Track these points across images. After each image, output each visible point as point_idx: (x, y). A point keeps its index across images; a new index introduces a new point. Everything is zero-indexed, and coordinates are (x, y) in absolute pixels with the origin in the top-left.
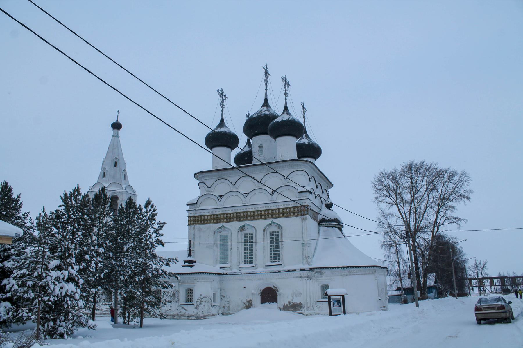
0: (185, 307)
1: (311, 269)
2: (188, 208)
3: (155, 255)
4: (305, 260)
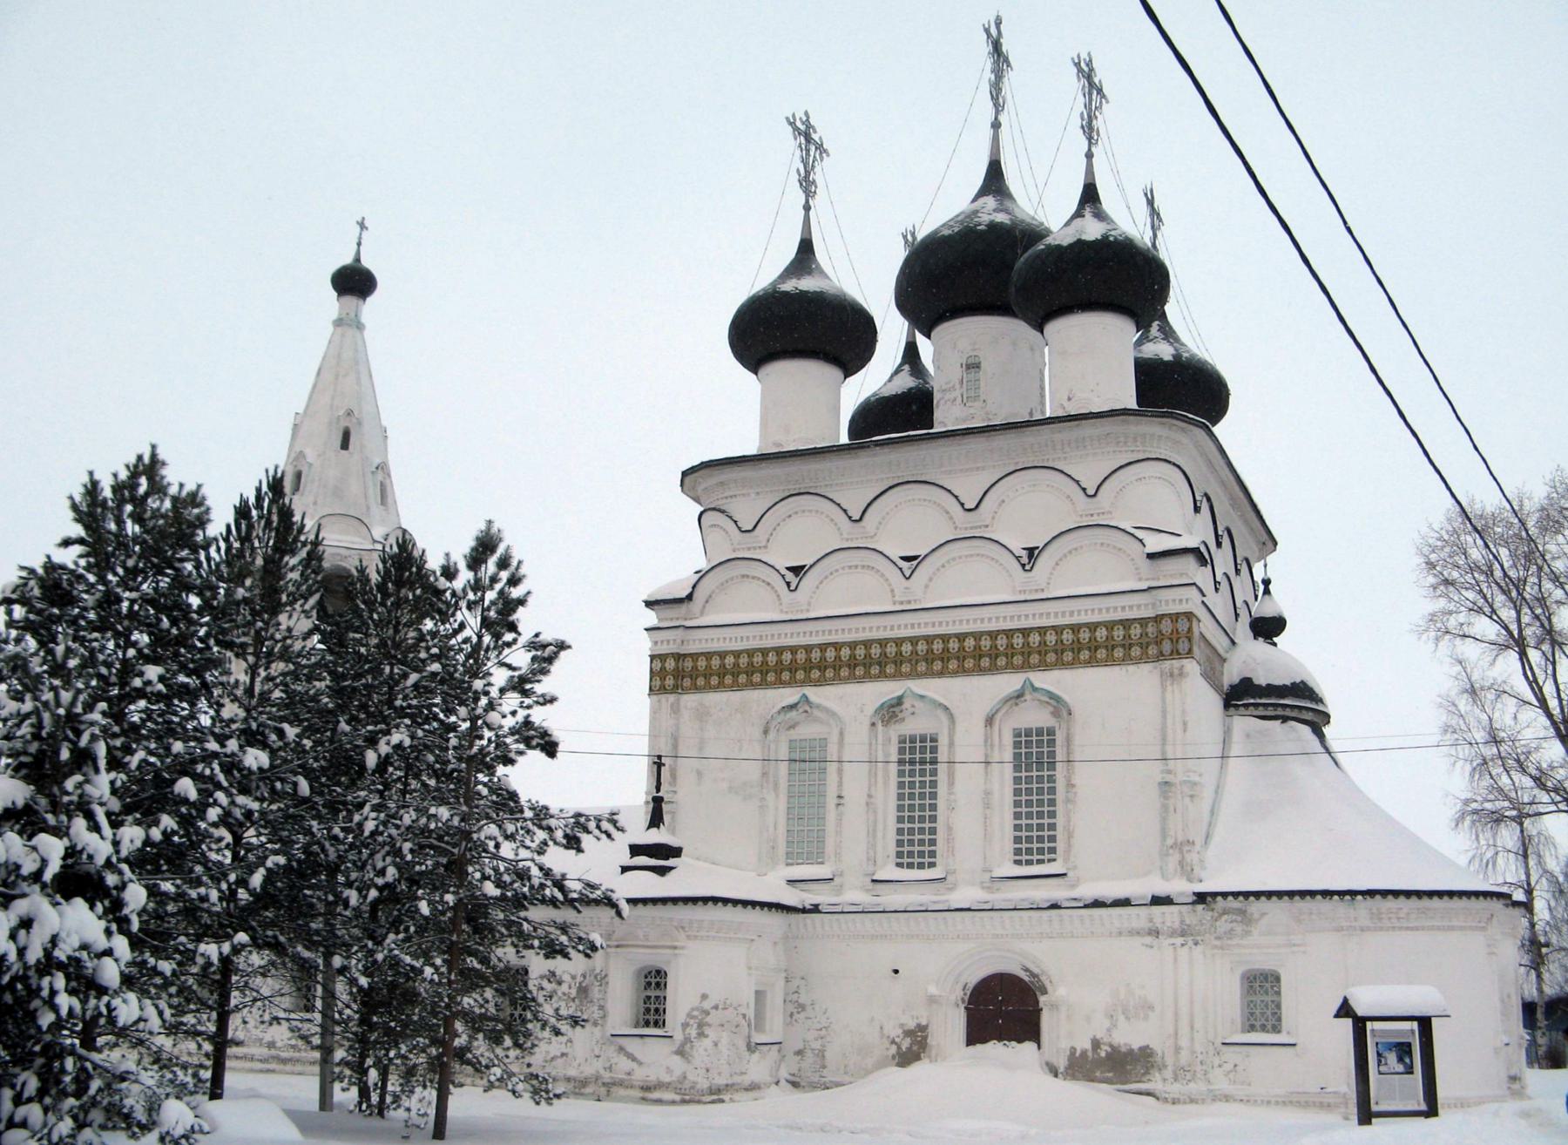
0: (633, 1046)
1: (1201, 898)
2: (651, 618)
3: (513, 796)
4: (1174, 859)
